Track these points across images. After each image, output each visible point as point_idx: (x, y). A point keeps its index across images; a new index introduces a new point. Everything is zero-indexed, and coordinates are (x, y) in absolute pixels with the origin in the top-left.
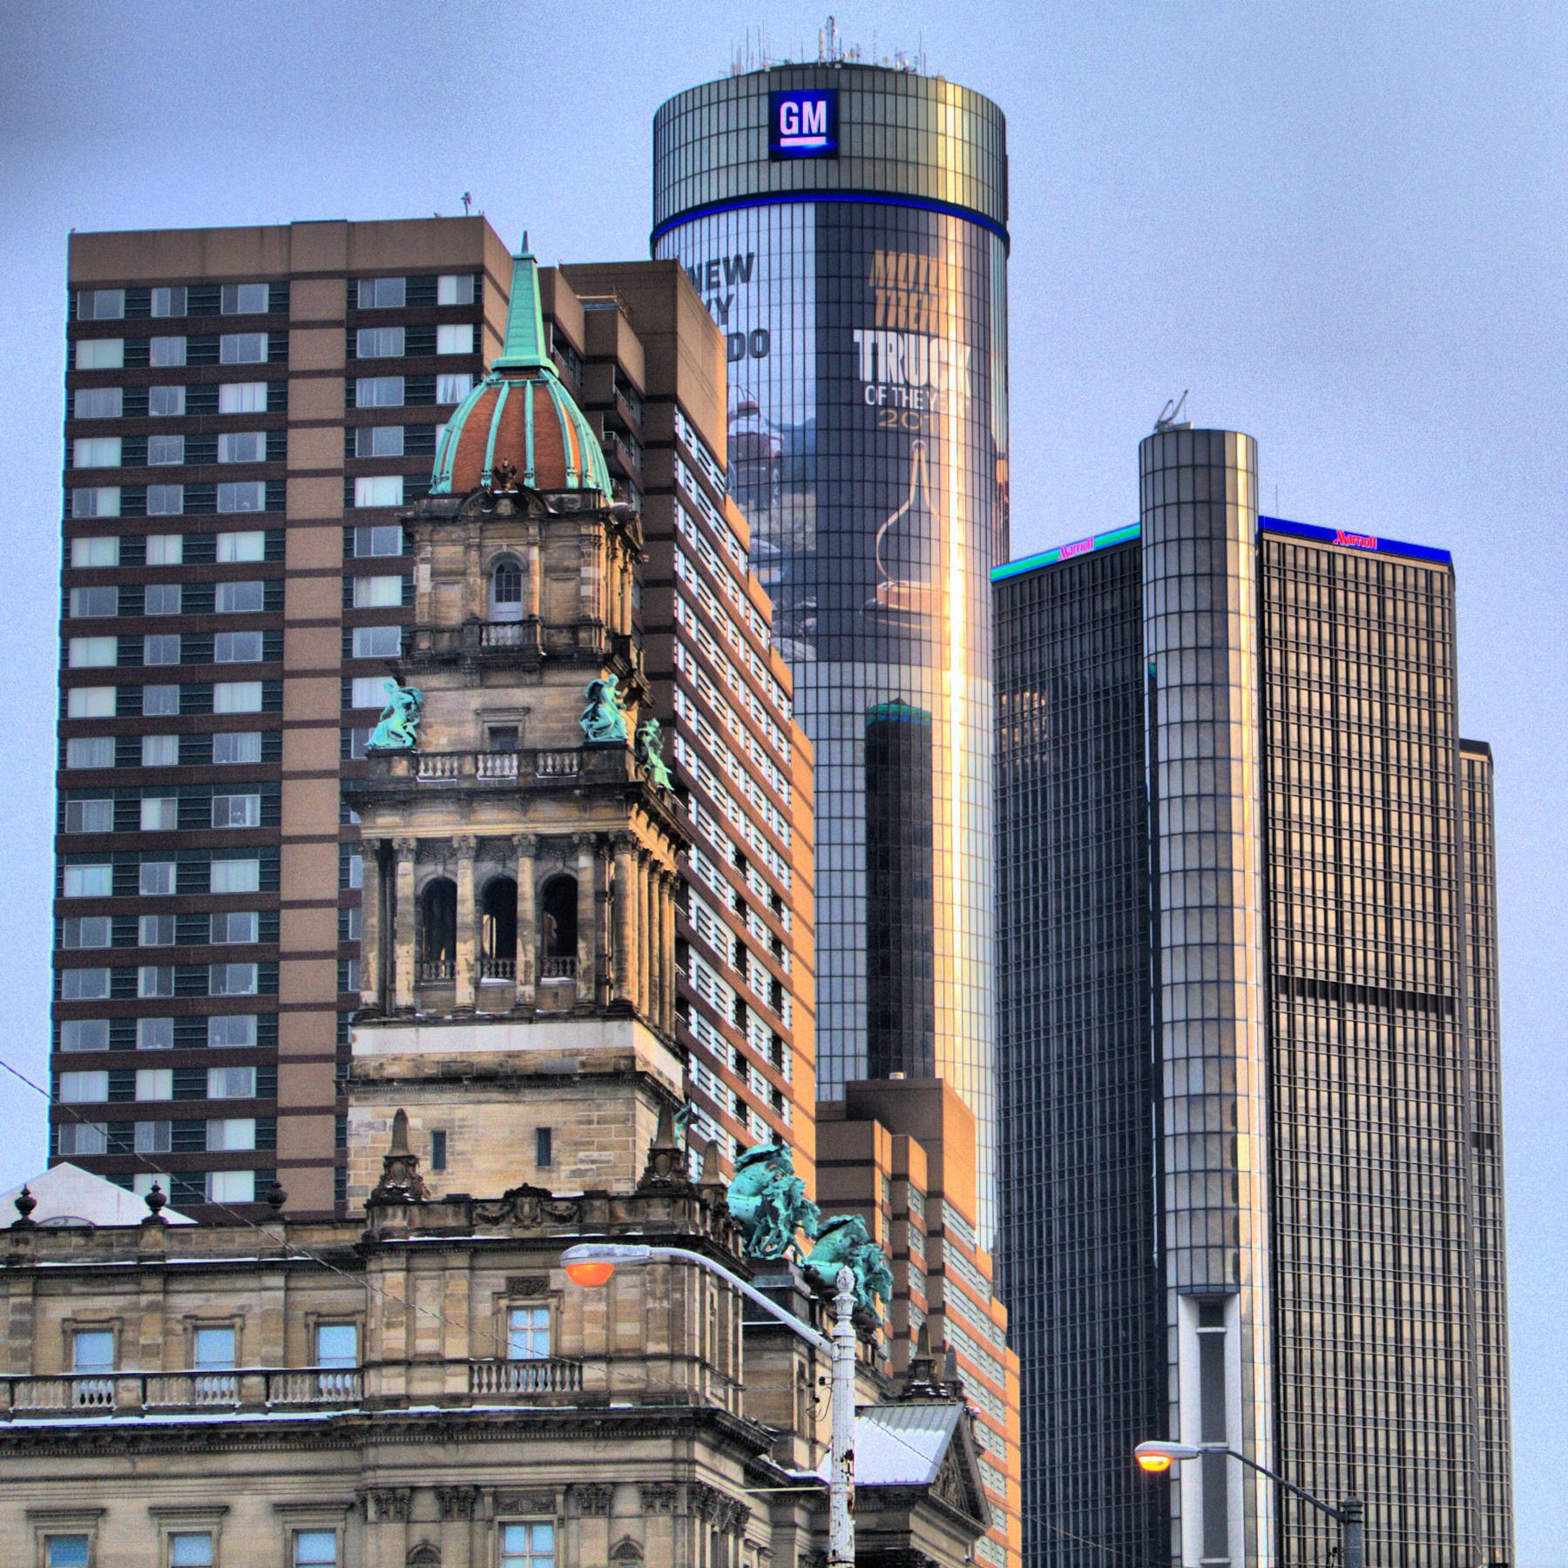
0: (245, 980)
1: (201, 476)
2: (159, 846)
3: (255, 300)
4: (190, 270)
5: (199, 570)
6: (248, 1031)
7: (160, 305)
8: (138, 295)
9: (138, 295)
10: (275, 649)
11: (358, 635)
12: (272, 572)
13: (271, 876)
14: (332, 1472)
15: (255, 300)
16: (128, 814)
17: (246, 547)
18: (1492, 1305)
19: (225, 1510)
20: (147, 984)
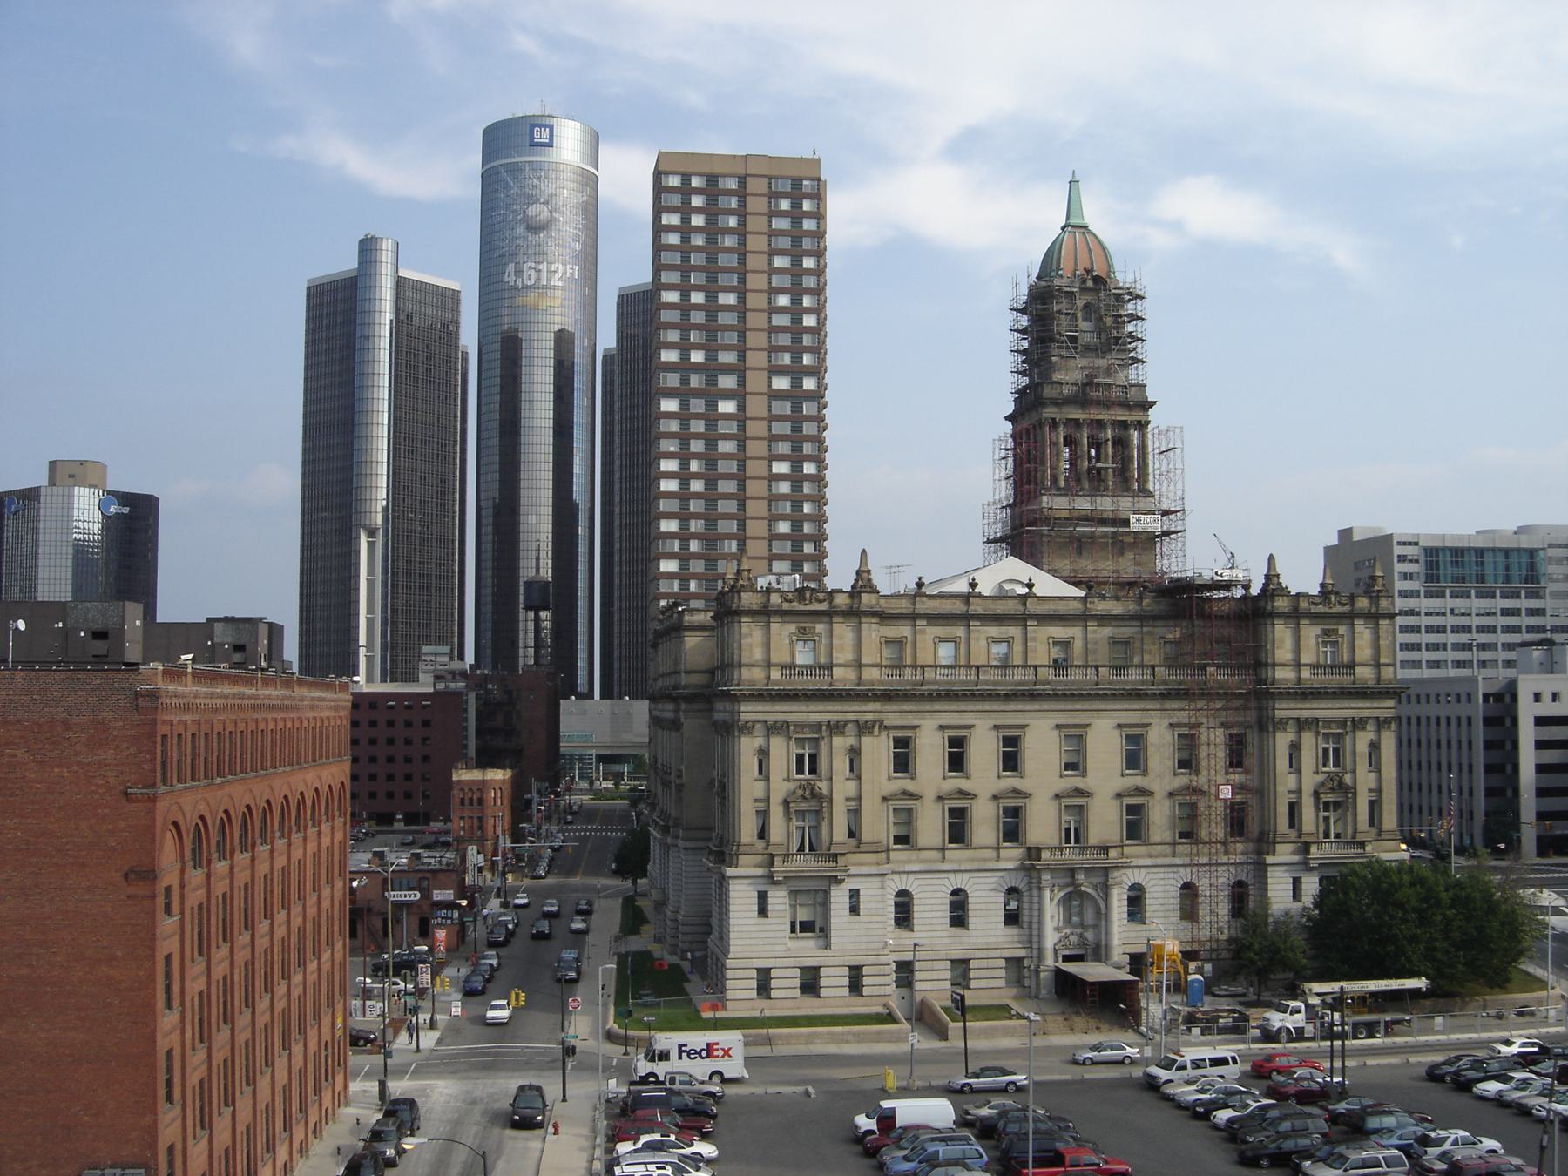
0: (732, 338)
1: (712, 271)
2: (697, 393)
3: (732, 184)
4: (707, 170)
5: (711, 308)
6: (733, 467)
7: (695, 182)
8: (686, 179)
9: (686, 179)
10: (743, 281)
11: (774, 316)
12: (741, 309)
13: (742, 407)
14: (290, 1073)
15: (732, 184)
16: (685, 380)
17: (729, 299)
18: (176, 988)
19: (1088, 725)
20: (694, 466)
